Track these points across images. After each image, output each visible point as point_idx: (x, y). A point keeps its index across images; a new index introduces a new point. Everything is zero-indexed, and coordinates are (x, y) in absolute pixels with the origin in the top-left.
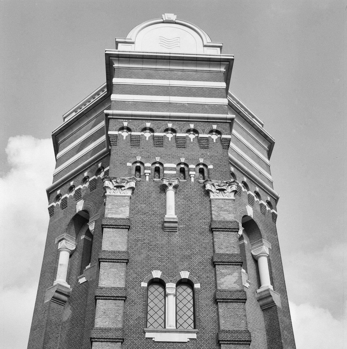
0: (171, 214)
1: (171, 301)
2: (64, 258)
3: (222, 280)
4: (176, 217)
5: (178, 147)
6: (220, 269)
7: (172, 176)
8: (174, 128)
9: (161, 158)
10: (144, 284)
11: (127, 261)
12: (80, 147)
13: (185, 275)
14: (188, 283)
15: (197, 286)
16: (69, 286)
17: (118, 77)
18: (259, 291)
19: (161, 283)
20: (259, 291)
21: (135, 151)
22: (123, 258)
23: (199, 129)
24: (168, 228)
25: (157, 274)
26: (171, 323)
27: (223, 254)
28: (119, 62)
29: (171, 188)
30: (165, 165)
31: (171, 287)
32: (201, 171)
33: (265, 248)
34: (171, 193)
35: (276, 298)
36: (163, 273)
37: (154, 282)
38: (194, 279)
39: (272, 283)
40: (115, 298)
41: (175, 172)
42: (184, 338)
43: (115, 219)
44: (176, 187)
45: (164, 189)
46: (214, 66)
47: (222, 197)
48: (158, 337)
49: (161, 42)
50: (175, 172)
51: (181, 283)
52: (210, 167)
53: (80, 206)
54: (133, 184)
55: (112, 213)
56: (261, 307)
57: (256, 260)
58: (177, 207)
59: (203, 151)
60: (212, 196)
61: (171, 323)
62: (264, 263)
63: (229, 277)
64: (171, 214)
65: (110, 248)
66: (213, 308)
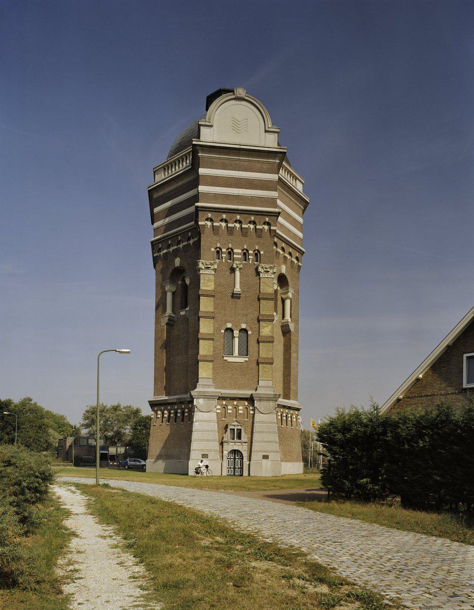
1: (236, 340)
2: (169, 296)
7: (238, 259)
10: (223, 331)
13: (244, 326)
15: (250, 333)
16: (174, 316)
18: (283, 321)
24: (235, 296)
25: (229, 325)
26: (236, 352)
29: (238, 269)
30: (235, 251)
31: (236, 333)
32: (256, 255)
34: (238, 273)
37: (227, 329)
38: (248, 329)
39: (291, 317)
41: (240, 256)
42: (242, 360)
44: (240, 269)
45: (233, 270)
46: (271, 158)
48: (230, 359)
50: (240, 256)
52: (262, 253)
54: (216, 267)
57: (283, 301)
59: (258, 240)
61: (236, 352)
66: (257, 345)
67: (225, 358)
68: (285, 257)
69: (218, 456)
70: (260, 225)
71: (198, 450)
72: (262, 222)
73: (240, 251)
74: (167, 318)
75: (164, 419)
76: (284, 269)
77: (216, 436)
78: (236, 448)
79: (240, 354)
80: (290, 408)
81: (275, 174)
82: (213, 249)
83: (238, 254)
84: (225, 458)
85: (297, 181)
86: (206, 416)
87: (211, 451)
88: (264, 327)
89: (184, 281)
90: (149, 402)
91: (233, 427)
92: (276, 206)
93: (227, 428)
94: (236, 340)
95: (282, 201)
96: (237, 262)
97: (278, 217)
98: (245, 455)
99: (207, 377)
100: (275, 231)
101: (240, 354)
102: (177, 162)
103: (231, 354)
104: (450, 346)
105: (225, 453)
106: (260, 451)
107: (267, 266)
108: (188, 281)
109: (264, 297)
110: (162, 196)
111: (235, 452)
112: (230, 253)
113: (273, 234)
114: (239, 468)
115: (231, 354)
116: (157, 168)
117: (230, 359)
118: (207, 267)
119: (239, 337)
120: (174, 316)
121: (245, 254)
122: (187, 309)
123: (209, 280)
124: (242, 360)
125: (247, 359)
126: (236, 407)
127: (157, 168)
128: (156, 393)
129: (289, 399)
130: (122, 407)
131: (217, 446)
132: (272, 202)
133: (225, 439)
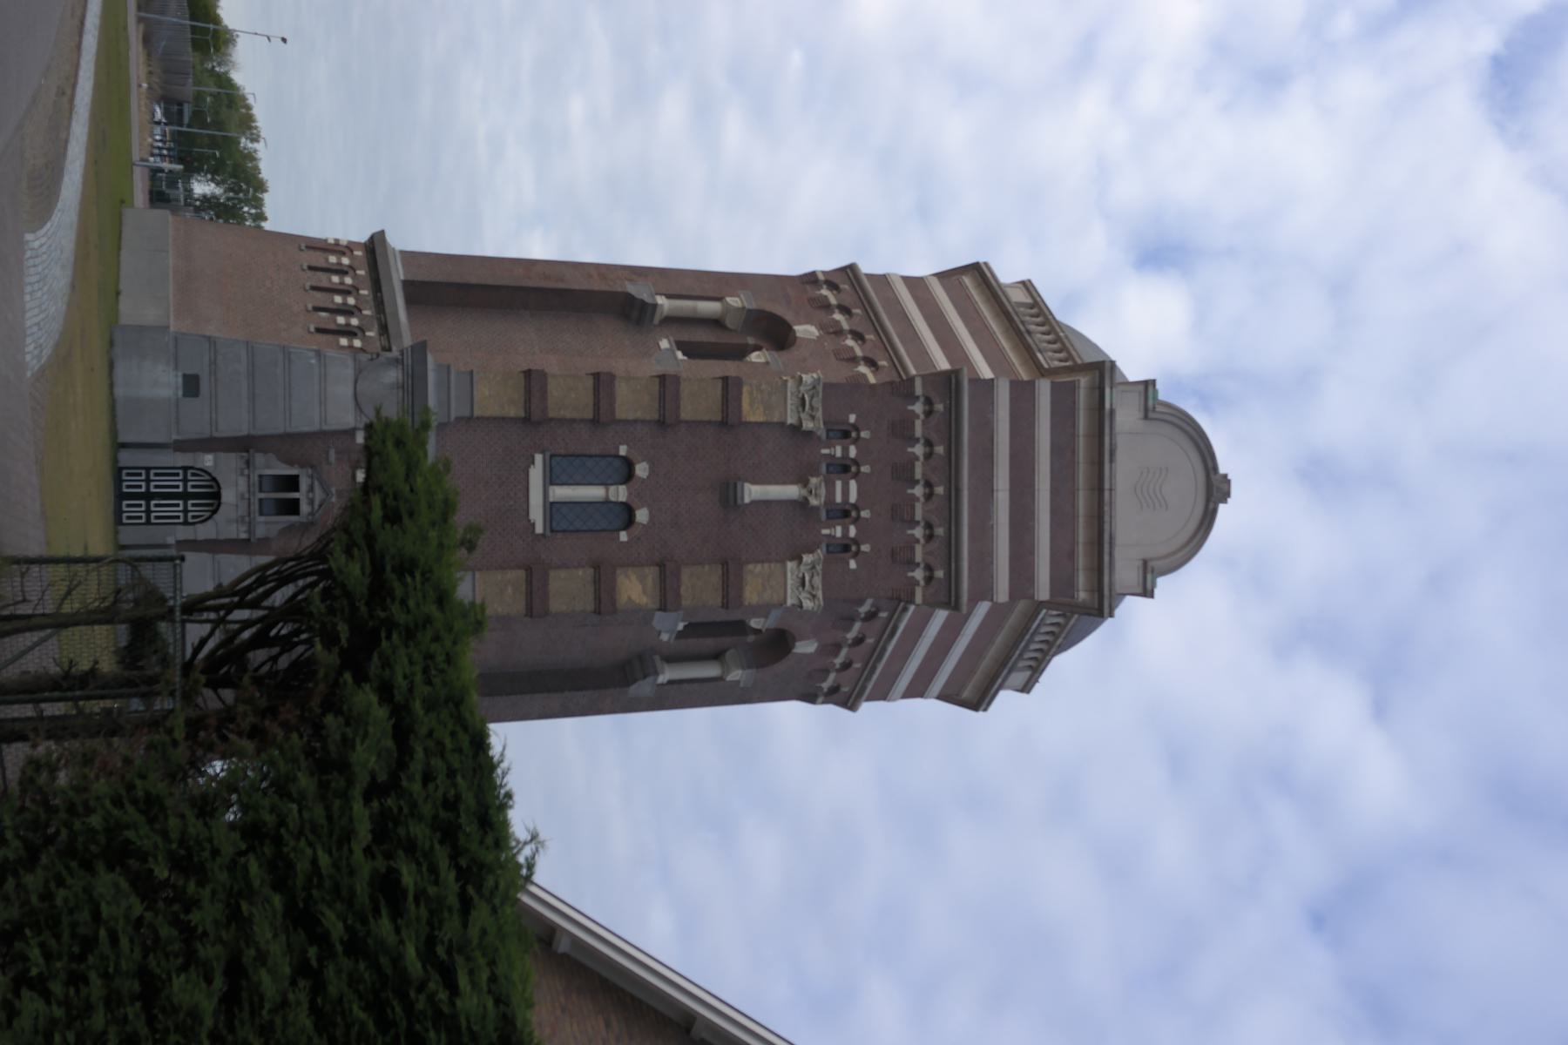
0: (753, 492)
3: (633, 578)
4: (747, 500)
6: (651, 573)
10: (623, 450)
13: (642, 516)
14: (629, 522)
16: (657, 320)
18: (657, 658)
19: (628, 476)
20: (657, 658)
23: (934, 545)
24: (728, 494)
25: (642, 470)
26: (560, 493)
28: (1091, 388)
31: (620, 493)
33: (736, 675)
35: (643, 688)
36: (643, 480)
37: (629, 464)
38: (635, 530)
39: (671, 682)
40: (597, 404)
41: (839, 499)
42: (537, 514)
43: (739, 399)
47: (790, 582)
48: (536, 474)
50: (839, 499)
51: (628, 510)
53: (806, 331)
55: (751, 393)
57: (716, 656)
58: (767, 504)
60: (790, 565)
61: (560, 493)
62: (710, 670)
63: (640, 587)
64: (753, 492)
67: (539, 458)
68: (837, 647)
70: (925, 554)
71: (213, 363)
73: (853, 498)
74: (645, 297)
76: (806, 647)
77: (272, 422)
78: (228, 496)
80: (379, 305)
82: (852, 418)
83: (846, 492)
84: (182, 459)
85: (1028, 673)
86: (342, 390)
89: (758, 348)
90: (382, 233)
91: (304, 484)
92: (974, 601)
93: (302, 466)
94: (594, 493)
95: (988, 615)
96: (823, 491)
97: (946, 605)
99: (476, 399)
100: (911, 601)
101: (552, 508)
102: (1034, 311)
104: (688, 1031)
105: (208, 461)
106: (213, 363)
107: (818, 581)
108: (755, 357)
110: (968, 297)
111: (213, 496)
112: (844, 468)
113: (902, 599)
115: (551, 479)
117: (536, 474)
118: (803, 399)
119: (606, 502)
120: (657, 320)
121: (844, 513)
122: (680, 355)
124: (537, 514)
125: (539, 529)
128: (410, 257)
131: (235, 423)
132: (983, 590)
133: (259, 459)
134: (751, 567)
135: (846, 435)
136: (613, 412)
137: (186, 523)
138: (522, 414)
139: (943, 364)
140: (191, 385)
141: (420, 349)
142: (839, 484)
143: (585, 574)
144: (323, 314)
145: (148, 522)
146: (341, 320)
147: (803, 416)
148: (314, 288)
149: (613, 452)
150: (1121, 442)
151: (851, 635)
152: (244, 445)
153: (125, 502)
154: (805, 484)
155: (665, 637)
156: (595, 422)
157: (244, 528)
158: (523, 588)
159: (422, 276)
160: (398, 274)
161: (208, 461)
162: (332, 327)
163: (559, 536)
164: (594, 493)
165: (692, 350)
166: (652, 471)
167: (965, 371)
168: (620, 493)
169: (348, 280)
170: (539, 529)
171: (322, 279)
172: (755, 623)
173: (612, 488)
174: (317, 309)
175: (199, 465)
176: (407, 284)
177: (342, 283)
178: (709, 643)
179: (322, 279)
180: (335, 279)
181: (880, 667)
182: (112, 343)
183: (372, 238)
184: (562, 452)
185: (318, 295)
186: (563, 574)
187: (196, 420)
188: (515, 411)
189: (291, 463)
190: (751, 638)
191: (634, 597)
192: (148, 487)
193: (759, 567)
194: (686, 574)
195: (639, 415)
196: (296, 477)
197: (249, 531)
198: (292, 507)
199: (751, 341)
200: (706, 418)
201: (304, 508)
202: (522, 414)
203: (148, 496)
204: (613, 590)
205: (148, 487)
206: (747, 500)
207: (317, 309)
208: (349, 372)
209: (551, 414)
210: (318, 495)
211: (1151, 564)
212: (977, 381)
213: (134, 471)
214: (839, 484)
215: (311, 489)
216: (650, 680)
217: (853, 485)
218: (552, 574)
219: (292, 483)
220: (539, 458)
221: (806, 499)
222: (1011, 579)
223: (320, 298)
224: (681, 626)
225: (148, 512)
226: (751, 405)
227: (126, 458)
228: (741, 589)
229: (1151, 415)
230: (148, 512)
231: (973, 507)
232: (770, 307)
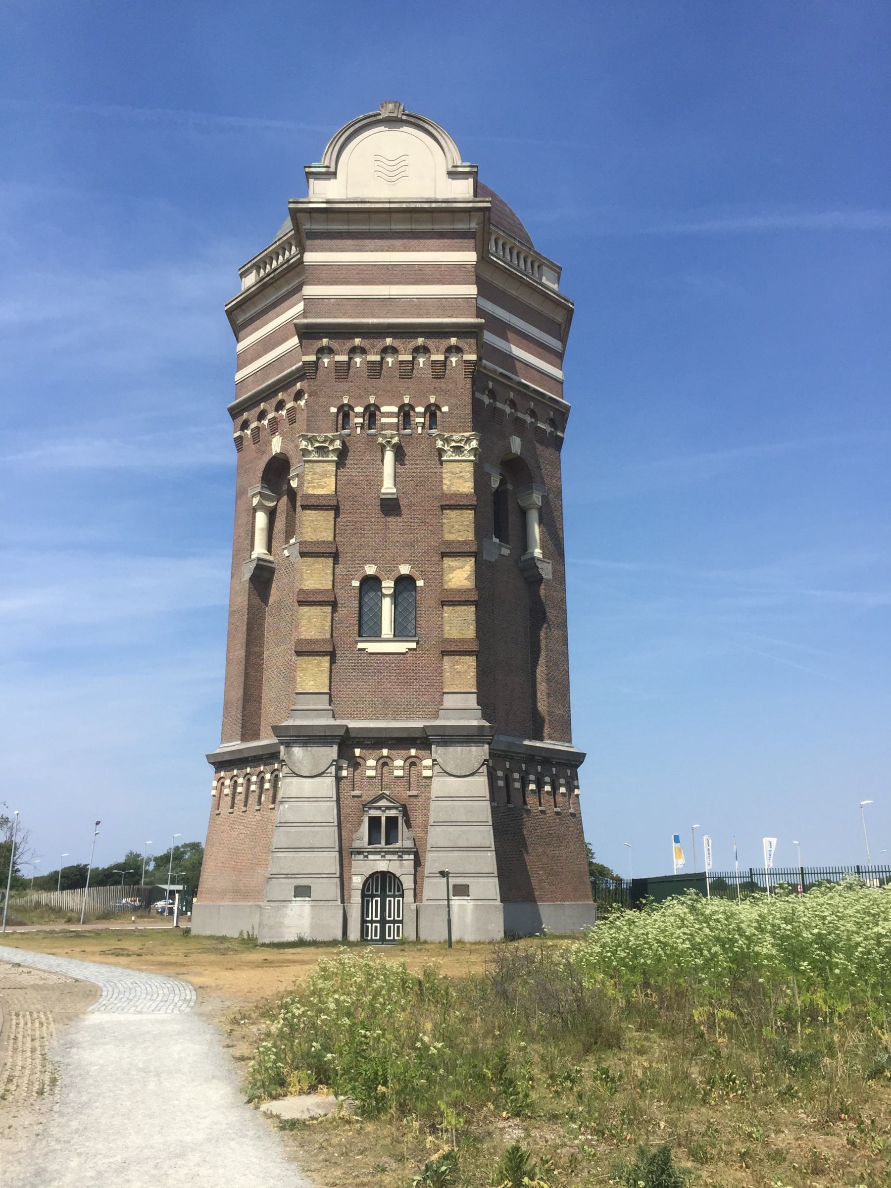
3: (451, 576)
4: (394, 491)
5: (402, 377)
6: (448, 562)
7: (390, 426)
8: (395, 345)
9: (377, 397)
11: (336, 557)
12: (550, 534)
13: (405, 569)
17: (312, 251)
19: (371, 583)
21: (343, 385)
22: (329, 550)
24: (390, 507)
26: (387, 629)
27: (453, 542)
30: (384, 409)
31: (388, 585)
33: (537, 498)
35: (546, 570)
38: (416, 575)
42: (401, 647)
48: (373, 647)
49: (379, 169)
50: (395, 420)
51: (404, 583)
52: (445, 409)
53: (276, 445)
55: (314, 487)
56: (229, 313)
57: (523, 513)
61: (387, 629)
65: (312, 536)
67: (361, 645)
69: (332, 889)
71: (287, 876)
72: (443, 348)
74: (253, 566)
75: (238, 798)
76: (516, 444)
77: (330, 836)
78: (382, 866)
79: (400, 633)
81: (469, 251)
83: (389, 415)
85: (544, 268)
86: (307, 787)
87: (318, 875)
88: (452, 569)
90: (207, 756)
94: (387, 605)
96: (388, 432)
98: (408, 882)
101: (400, 633)
102: (280, 252)
103: (375, 634)
106: (287, 876)
107: (456, 437)
109: (452, 502)
112: (372, 413)
114: (372, 922)
115: (375, 634)
116: (246, 267)
117: (373, 647)
121: (406, 413)
122: (292, 541)
123: (325, 475)
124: (401, 647)
125: (413, 645)
126: (384, 763)
127: (246, 267)
129: (541, 739)
130: (576, 792)
131: (329, 862)
134: (445, 488)
135: (346, 416)
136: (327, 591)
137: (402, 896)
138: (328, 658)
139: (295, 340)
140: (302, 891)
141: (277, 730)
142: (384, 420)
143: (448, 611)
144: (263, 798)
145: (401, 922)
146: (267, 786)
147: (331, 448)
148: (246, 806)
149: (357, 591)
150: (353, 194)
151: (508, 410)
152: (346, 854)
153: (387, 938)
154: (383, 448)
155: (505, 551)
156: (334, 605)
157: (406, 857)
158: (457, 658)
159: (238, 728)
160: (236, 745)
161: (357, 881)
162: (271, 792)
163: (418, 630)
164: (387, 605)
165: (290, 532)
166: (373, 561)
167: (296, 321)
168: (388, 585)
169: (240, 780)
170: (413, 645)
171: (240, 799)
172: (495, 483)
173: (384, 591)
174: (260, 803)
175: (361, 886)
176: (244, 738)
177: (270, 781)
178: (513, 519)
179: (240, 799)
180: (239, 789)
181: (294, 368)
182: (250, 942)
183: (213, 764)
184: (356, 628)
185: (250, 802)
186: (446, 628)
187: (328, 889)
188: (325, 661)
189: (360, 822)
190: (510, 487)
191: (466, 576)
192: (376, 922)
193: (445, 481)
194: (449, 537)
195: (330, 571)
196: (370, 818)
197: (409, 853)
198: (392, 822)
199: (285, 488)
200: (332, 522)
201: (393, 813)
202: (328, 658)
203: (383, 922)
204: (459, 591)
205: (376, 922)
206: (394, 491)
207: (260, 803)
208: (296, 780)
209: (328, 636)
210: (383, 803)
211: (451, 169)
212: (305, 314)
213: (364, 931)
214: (384, 420)
215: (379, 808)
216: (539, 565)
217: (384, 409)
218: (446, 636)
219: (374, 822)
220: (361, 645)
221: (394, 446)
222: (459, 283)
223: (253, 799)
224: (496, 540)
225: (394, 922)
226: (323, 487)
227: (354, 934)
228: (462, 495)
229: (332, 169)
230: (394, 922)
231: (403, 314)
232: (260, 474)
